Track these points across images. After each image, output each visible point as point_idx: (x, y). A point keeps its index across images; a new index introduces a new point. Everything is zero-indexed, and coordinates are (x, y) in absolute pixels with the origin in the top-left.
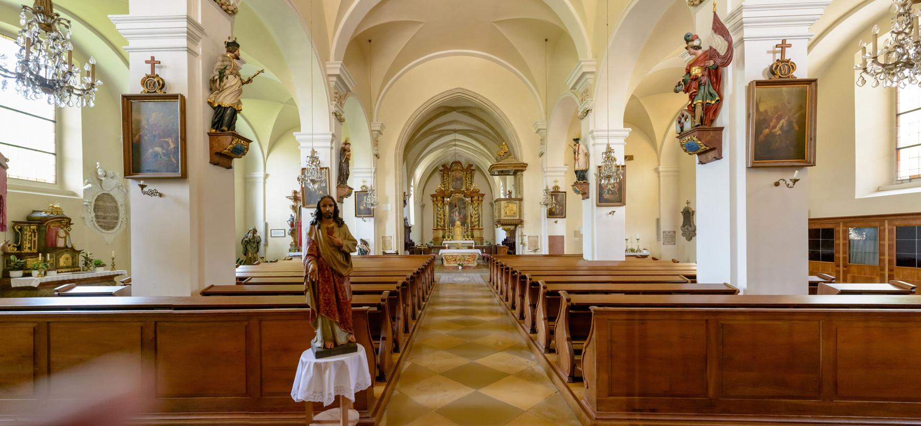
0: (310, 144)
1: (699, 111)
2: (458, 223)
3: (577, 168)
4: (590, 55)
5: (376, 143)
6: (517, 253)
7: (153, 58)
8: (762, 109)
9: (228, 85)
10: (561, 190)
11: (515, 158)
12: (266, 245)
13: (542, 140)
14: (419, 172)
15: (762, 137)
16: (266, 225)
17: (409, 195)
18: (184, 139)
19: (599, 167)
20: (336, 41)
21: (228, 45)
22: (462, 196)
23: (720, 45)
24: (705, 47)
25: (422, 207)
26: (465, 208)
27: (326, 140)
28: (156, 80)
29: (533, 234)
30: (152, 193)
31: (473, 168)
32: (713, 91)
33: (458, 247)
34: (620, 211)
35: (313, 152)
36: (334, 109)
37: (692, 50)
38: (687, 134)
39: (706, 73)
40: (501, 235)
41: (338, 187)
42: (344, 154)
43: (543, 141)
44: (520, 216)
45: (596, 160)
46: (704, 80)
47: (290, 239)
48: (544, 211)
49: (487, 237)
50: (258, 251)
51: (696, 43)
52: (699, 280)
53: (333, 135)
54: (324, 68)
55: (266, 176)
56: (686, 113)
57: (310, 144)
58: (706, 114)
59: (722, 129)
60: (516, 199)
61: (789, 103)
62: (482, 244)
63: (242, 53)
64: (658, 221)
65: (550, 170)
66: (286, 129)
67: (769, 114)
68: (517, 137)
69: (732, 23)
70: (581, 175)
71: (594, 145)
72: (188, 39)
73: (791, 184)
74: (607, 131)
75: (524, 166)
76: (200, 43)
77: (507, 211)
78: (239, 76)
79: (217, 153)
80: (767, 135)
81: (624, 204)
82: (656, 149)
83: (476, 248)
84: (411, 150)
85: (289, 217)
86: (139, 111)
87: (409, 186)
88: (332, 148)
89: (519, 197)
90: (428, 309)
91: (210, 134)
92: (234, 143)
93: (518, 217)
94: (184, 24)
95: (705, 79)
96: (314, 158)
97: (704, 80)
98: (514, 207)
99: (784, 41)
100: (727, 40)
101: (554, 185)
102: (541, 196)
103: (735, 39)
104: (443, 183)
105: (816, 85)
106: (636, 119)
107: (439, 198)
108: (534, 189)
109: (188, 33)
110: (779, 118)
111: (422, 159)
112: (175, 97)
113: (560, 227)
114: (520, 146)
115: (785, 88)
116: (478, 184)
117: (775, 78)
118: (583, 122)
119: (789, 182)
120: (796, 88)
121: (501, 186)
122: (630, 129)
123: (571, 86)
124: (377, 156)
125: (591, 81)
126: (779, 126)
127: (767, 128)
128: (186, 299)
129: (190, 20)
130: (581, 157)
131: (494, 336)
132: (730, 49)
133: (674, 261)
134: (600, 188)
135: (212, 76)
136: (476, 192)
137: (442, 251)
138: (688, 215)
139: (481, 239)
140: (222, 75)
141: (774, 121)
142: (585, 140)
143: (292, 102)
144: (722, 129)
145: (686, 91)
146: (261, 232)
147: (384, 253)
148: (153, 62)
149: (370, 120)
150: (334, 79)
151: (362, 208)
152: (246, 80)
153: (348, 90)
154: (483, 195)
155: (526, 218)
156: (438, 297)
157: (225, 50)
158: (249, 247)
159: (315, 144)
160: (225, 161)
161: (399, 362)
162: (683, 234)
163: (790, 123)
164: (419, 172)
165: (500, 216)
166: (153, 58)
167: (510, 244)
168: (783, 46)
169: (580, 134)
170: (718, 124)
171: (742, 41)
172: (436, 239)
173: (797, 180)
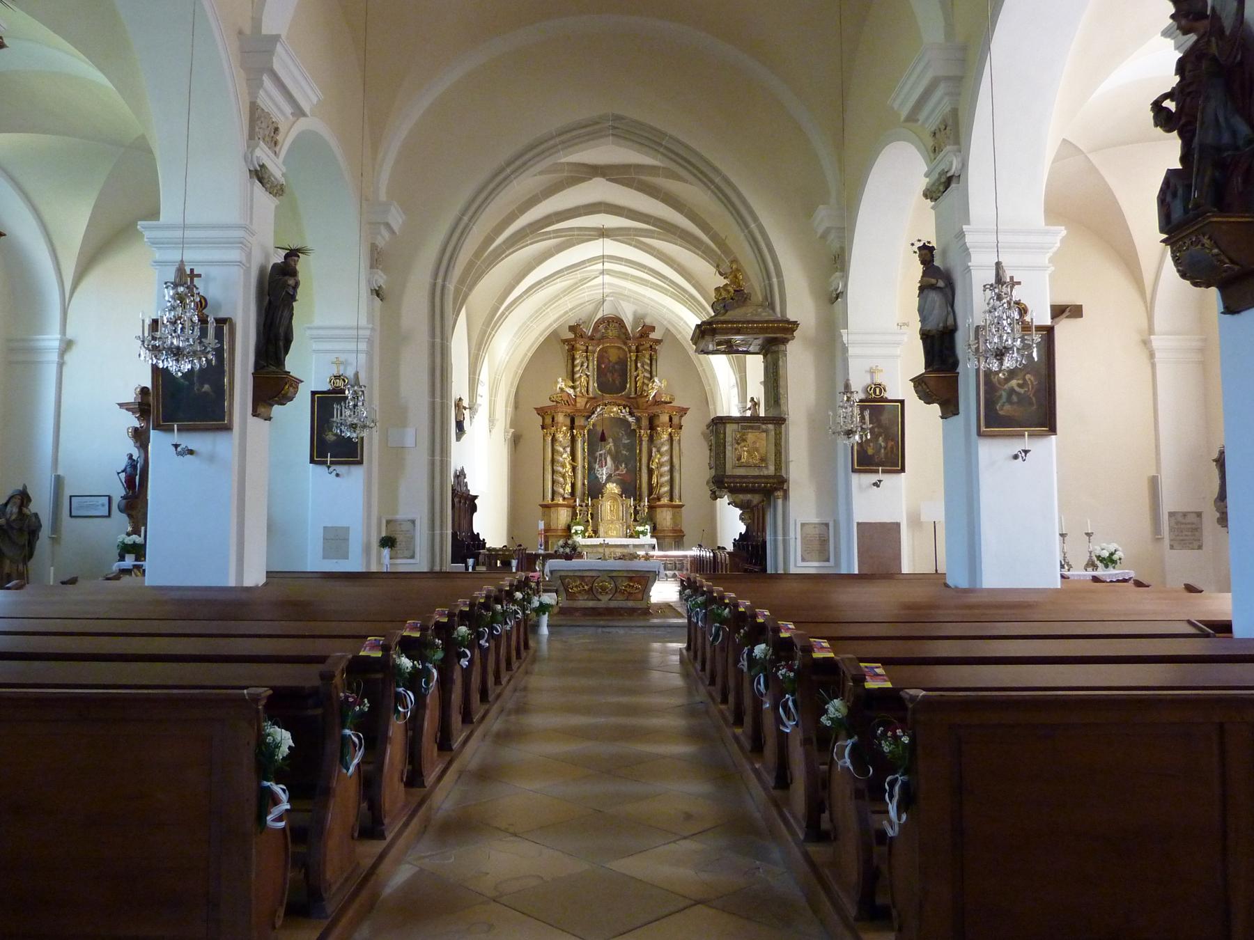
2: (613, 488)
6: (769, 571)
12: (55, 540)
16: (59, 482)
31: (653, 336)
34: (1045, 449)
40: (731, 524)
42: (278, 290)
44: (778, 466)
50: (31, 555)
52: (1238, 632)
55: (67, 345)
57: (175, 256)
60: (765, 420)
64: (1154, 483)
85: (123, 462)
93: (771, 470)
98: (760, 441)
101: (867, 380)
123: (904, 114)
133: (1190, 589)
134: (990, 384)
146: (41, 505)
154: (683, 411)
161: (375, 866)
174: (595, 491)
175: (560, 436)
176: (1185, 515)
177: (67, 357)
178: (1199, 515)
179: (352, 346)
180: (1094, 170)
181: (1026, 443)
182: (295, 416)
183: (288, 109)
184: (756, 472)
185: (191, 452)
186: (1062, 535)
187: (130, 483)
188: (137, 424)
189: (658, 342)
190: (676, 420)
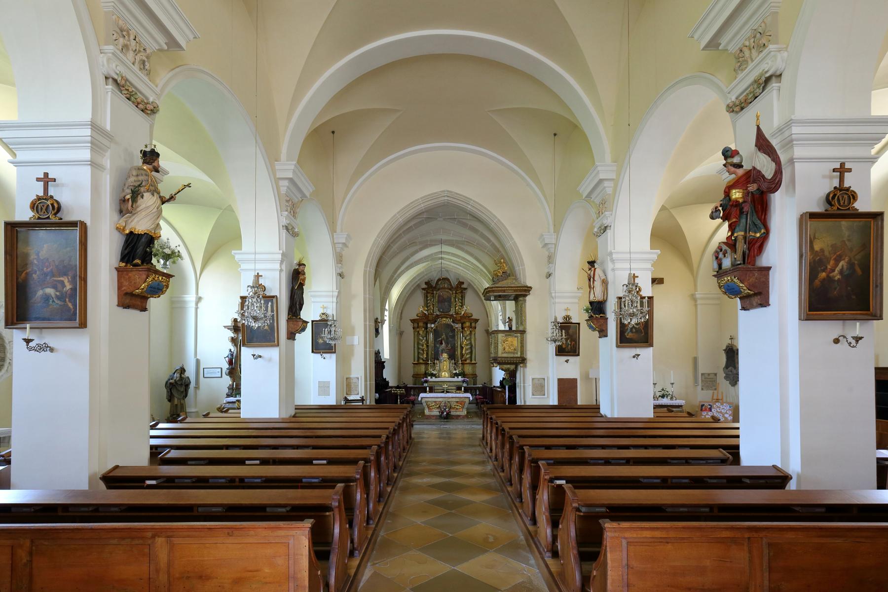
0: (252, 266)
1: (741, 246)
2: (445, 355)
3: (592, 298)
4: (608, 158)
5: (339, 259)
6: (518, 403)
7: (46, 175)
8: (817, 247)
9: (143, 206)
10: (573, 321)
11: (516, 279)
12: (197, 387)
13: (549, 257)
14: (396, 292)
15: (817, 282)
16: (198, 362)
17: (383, 322)
18: (84, 279)
19: (620, 298)
20: (293, 129)
21: (144, 154)
22: (449, 321)
23: (767, 168)
24: (747, 166)
25: (398, 334)
26: (453, 337)
27: (273, 261)
28: (49, 203)
29: (537, 376)
30: (44, 348)
31: (464, 286)
32: (758, 222)
33: (445, 389)
34: (646, 353)
35: (258, 276)
36: (284, 222)
37: (732, 169)
38: (726, 273)
39: (749, 199)
40: (499, 375)
41: (289, 320)
42: (297, 279)
43: (551, 259)
44: (522, 352)
45: (617, 290)
46: (747, 203)
47: (227, 381)
48: (552, 348)
49: (480, 372)
50: (186, 396)
51: (736, 160)
53: (283, 255)
54: (272, 171)
55: (199, 299)
56: (724, 247)
58: (749, 249)
59: (769, 268)
60: (516, 331)
61: (849, 240)
62: (475, 383)
63: (162, 162)
64: (695, 360)
65: (559, 296)
66: (223, 242)
67: (827, 253)
68: (519, 253)
69: (779, 139)
70: (597, 309)
71: (613, 270)
72: (92, 149)
73: (853, 342)
74: (630, 254)
75: (528, 290)
76: (108, 154)
77: (505, 347)
78: (159, 193)
79: (126, 294)
80: (824, 279)
81: (651, 345)
82: (692, 273)
83: (466, 391)
84: (381, 271)
85: (227, 353)
86: (27, 242)
87: (383, 310)
88: (281, 271)
89: (521, 328)
90: (401, 484)
91: (118, 270)
92: (149, 279)
93: (519, 355)
94: (88, 132)
95: (747, 208)
96: (258, 287)
97: (747, 203)
98: (514, 341)
99: (842, 165)
100: (773, 160)
101: (564, 314)
102: (550, 331)
103: (783, 158)
104: (426, 305)
105: (882, 220)
106: (667, 236)
107: (421, 324)
108: (540, 318)
109: (92, 143)
110: (838, 260)
111: (399, 276)
112: (73, 224)
113: (570, 368)
114: (523, 265)
115: (844, 223)
116: (471, 306)
117: (834, 210)
118: (600, 240)
119: (850, 340)
120: (857, 223)
121: (500, 314)
122: (659, 251)
124: (341, 275)
125: (609, 191)
126: (838, 269)
127: (823, 271)
128: (82, 493)
129: (94, 126)
130: (598, 285)
131: (486, 526)
132: (778, 172)
135: (122, 195)
136: (468, 317)
137: (422, 395)
138: (732, 354)
139: (474, 376)
140: (136, 194)
141: (832, 262)
142: (602, 263)
143: (230, 210)
144: (769, 268)
145: (725, 218)
146: (190, 373)
147: (346, 400)
148: (46, 180)
149: (332, 230)
150: (286, 183)
151: (321, 341)
152: (168, 197)
153: (304, 196)
154: (476, 321)
155: (530, 355)
156: (417, 463)
157: (141, 161)
158: (174, 392)
159: (259, 266)
160: (138, 302)
162: (726, 378)
163: (851, 265)
164: (396, 292)
165: (497, 352)
166: (46, 175)
167: (510, 382)
168: (842, 170)
169: (596, 256)
170: (764, 260)
171: (791, 161)
172: (416, 376)
173: (861, 338)
174: (436, 357)
175: (421, 332)
176: (709, 374)
177: (199, 305)
178: (716, 374)
179: (331, 299)
180: (672, 216)
181: (638, 351)
182: (305, 339)
183: (299, 196)
184: (512, 355)
185: (260, 357)
186: (655, 384)
187: (230, 362)
188: (233, 335)
189: (465, 289)
190: (473, 325)
